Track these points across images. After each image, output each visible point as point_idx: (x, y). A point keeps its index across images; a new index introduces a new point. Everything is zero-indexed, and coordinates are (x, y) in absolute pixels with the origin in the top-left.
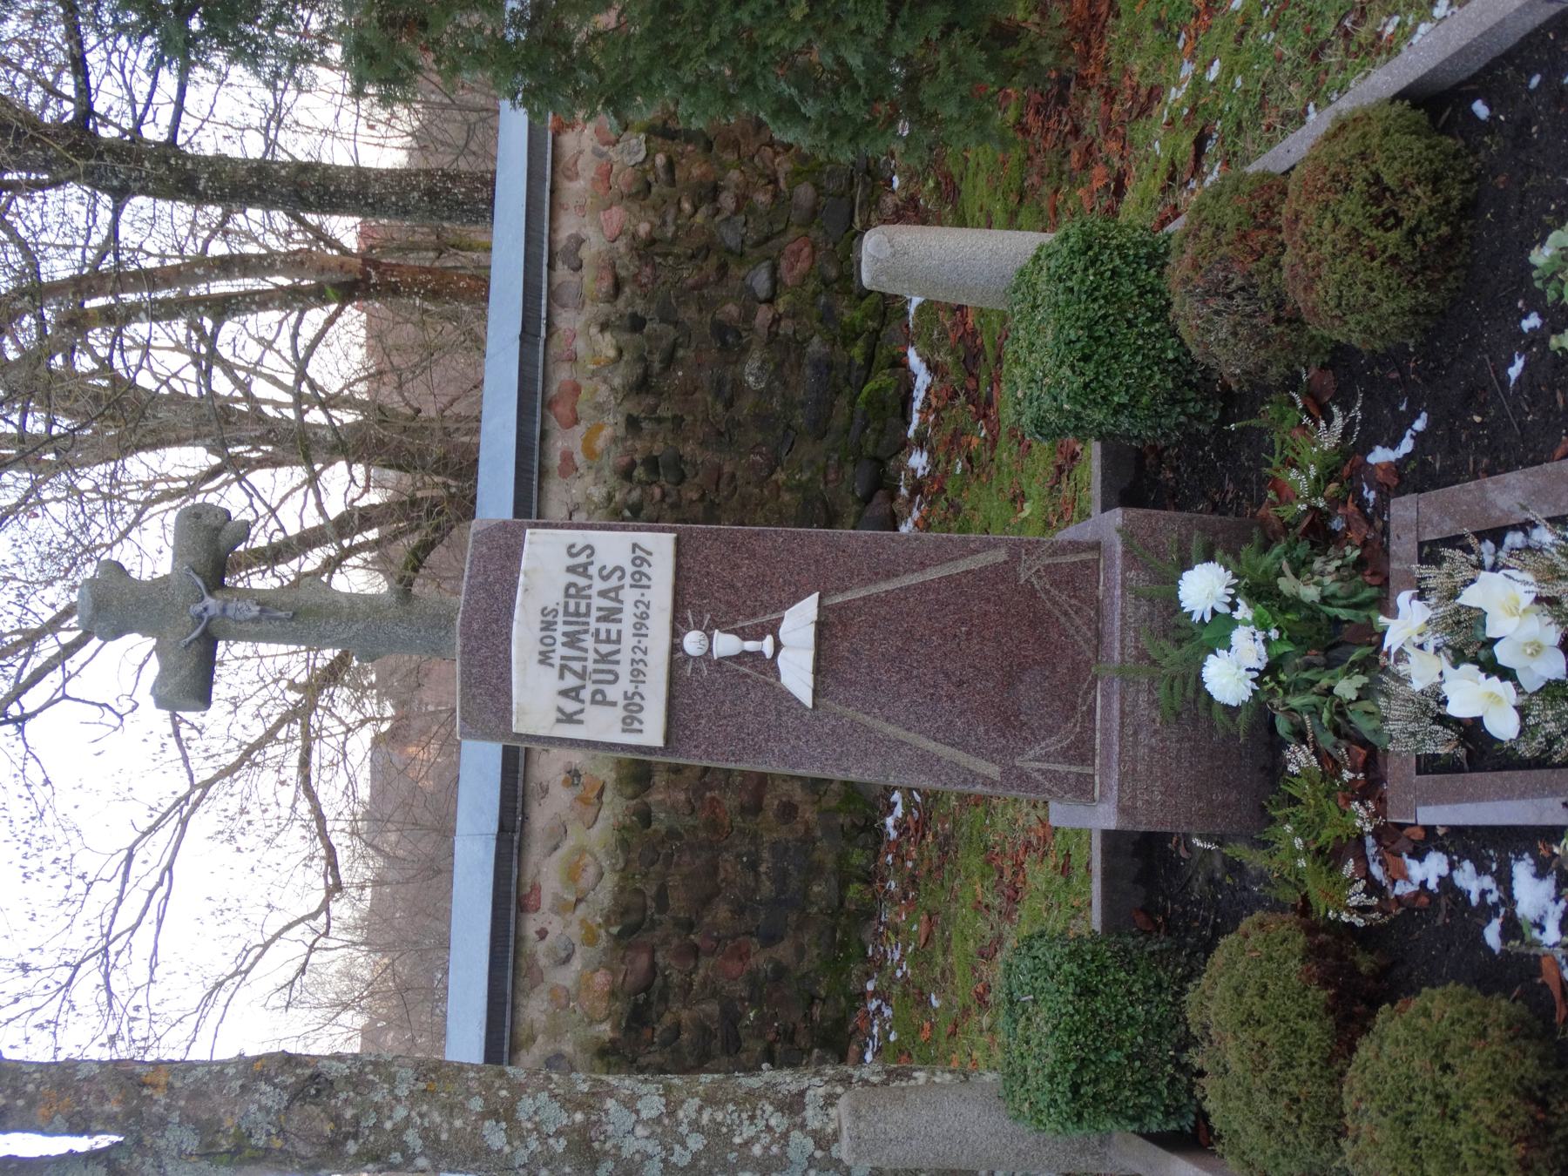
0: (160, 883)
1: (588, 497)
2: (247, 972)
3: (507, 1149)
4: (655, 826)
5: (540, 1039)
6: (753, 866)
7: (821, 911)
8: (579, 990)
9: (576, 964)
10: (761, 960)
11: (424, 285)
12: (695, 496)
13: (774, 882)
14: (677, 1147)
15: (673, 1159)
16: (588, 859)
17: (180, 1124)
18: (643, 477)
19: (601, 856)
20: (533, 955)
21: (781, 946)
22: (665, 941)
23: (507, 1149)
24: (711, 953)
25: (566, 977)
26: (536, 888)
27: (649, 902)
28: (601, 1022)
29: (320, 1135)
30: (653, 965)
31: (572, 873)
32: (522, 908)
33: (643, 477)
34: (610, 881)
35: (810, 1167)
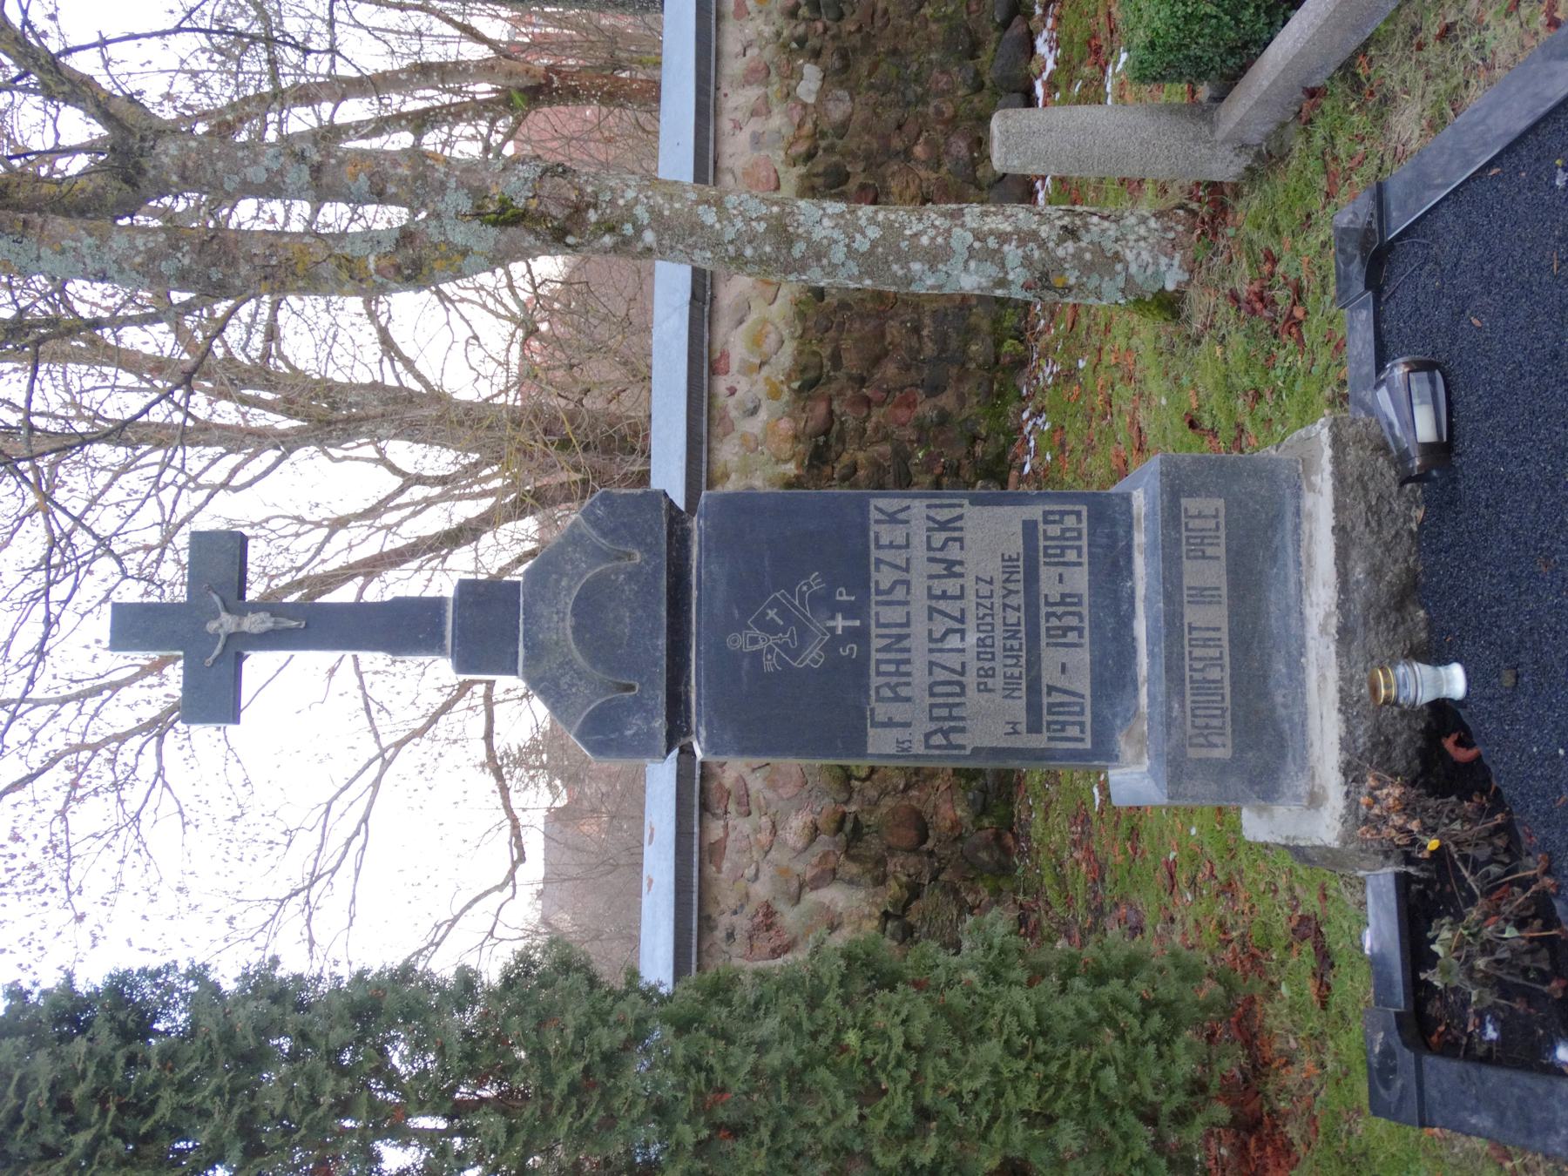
0: (357, 833)
1: (760, 34)
2: (438, 944)
3: (718, 226)
4: (827, 300)
5: (733, 476)
6: (916, 330)
7: (979, 367)
8: (766, 436)
9: (763, 415)
10: (926, 409)
11: (601, 87)
12: (853, 28)
13: (936, 343)
14: (858, 236)
15: (855, 245)
16: (770, 328)
17: (457, 189)
18: (807, 14)
19: (782, 326)
20: (724, 408)
21: (944, 396)
22: (840, 393)
23: (718, 226)
24: (881, 404)
25: (755, 426)
26: (725, 355)
27: (825, 361)
28: (786, 461)
29: (567, 199)
30: (831, 412)
31: (756, 340)
32: (713, 371)
33: (807, 14)
34: (790, 347)
35: (970, 257)
